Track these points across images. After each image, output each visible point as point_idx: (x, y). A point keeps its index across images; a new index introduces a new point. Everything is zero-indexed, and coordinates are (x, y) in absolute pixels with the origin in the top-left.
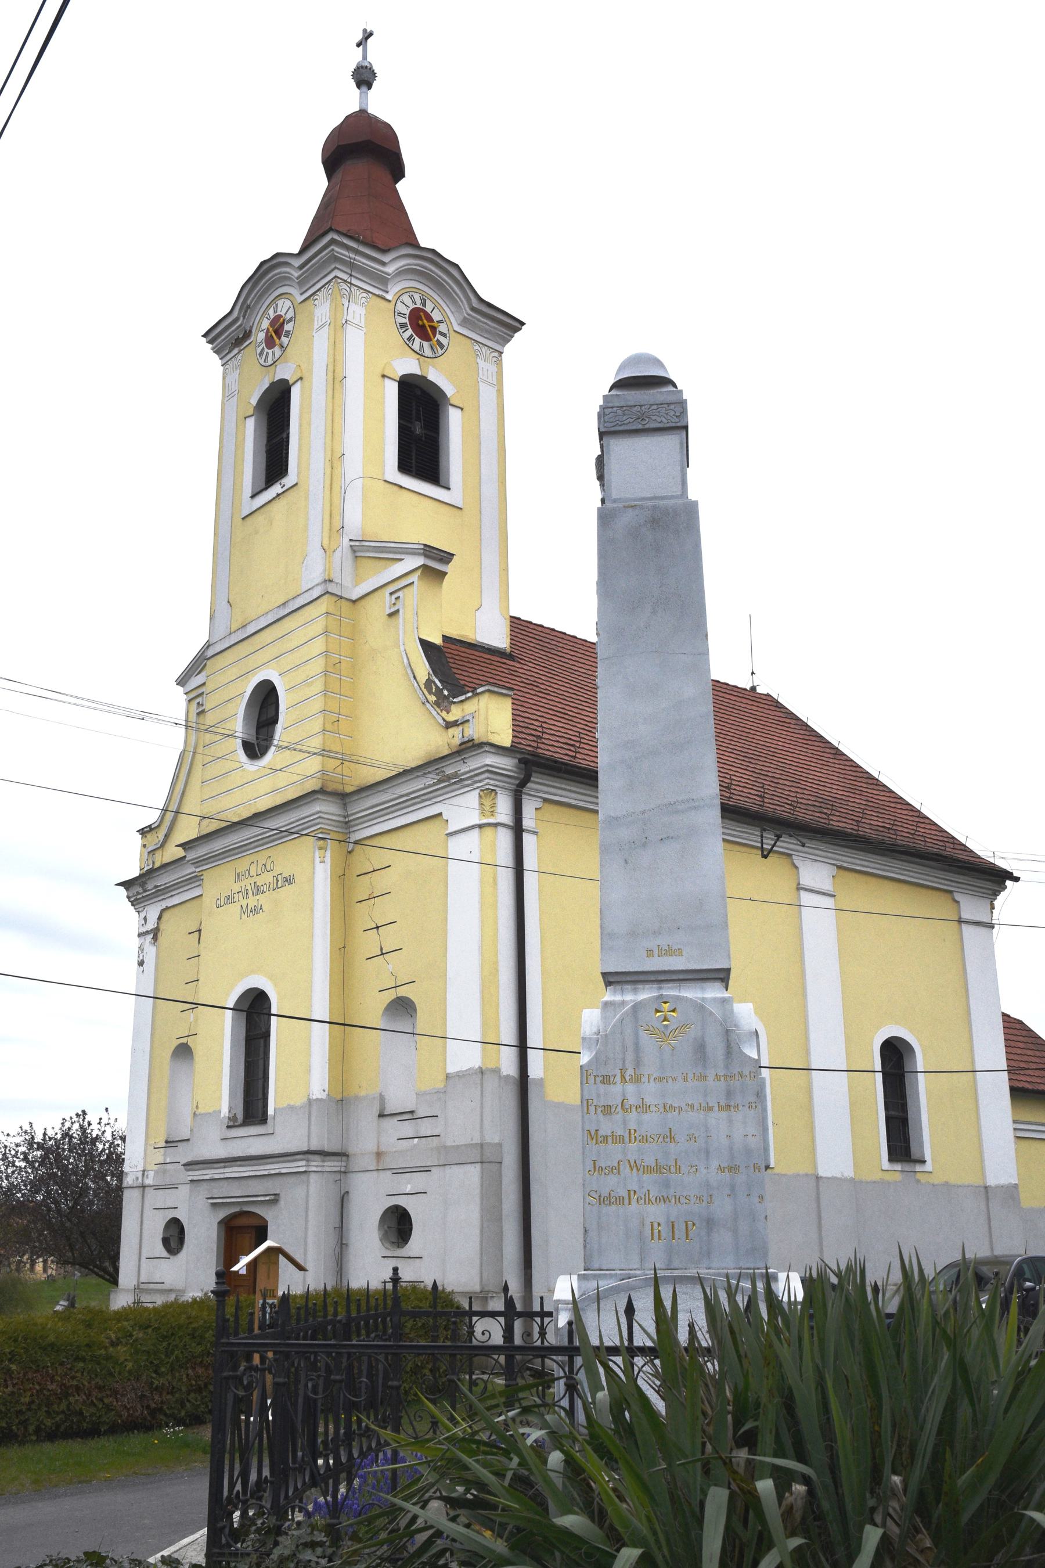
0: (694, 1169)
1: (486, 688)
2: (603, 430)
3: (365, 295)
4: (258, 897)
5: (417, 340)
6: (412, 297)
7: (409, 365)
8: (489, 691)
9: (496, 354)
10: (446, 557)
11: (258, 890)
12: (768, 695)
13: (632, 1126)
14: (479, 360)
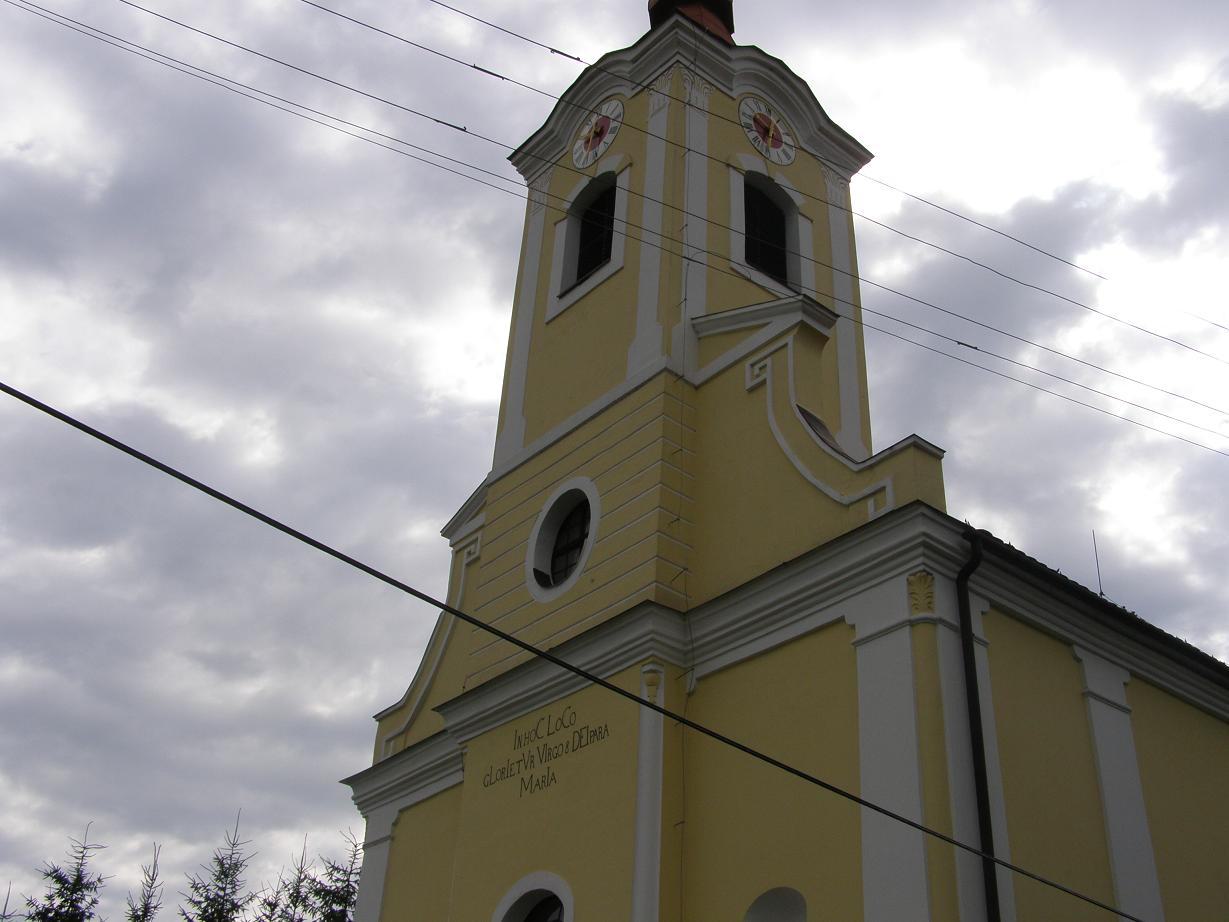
3: (708, 86)
4: (548, 764)
9: (843, 181)
11: (549, 754)
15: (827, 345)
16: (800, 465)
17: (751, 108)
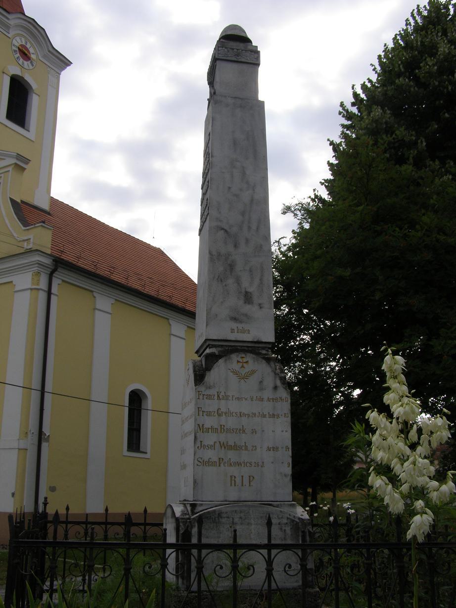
0: (254, 448)
1: (40, 224)
2: (216, 57)
5: (21, 60)
6: (21, 39)
7: (15, 70)
8: (42, 226)
9: (57, 74)
10: (27, 161)
12: (159, 248)
13: (223, 423)
14: (49, 75)
15: (25, 172)
16: (7, 221)
17: (18, 42)
